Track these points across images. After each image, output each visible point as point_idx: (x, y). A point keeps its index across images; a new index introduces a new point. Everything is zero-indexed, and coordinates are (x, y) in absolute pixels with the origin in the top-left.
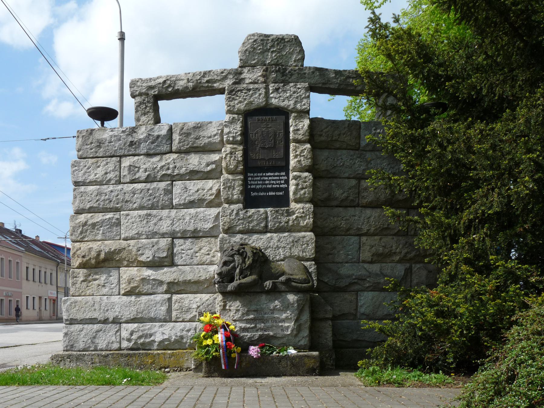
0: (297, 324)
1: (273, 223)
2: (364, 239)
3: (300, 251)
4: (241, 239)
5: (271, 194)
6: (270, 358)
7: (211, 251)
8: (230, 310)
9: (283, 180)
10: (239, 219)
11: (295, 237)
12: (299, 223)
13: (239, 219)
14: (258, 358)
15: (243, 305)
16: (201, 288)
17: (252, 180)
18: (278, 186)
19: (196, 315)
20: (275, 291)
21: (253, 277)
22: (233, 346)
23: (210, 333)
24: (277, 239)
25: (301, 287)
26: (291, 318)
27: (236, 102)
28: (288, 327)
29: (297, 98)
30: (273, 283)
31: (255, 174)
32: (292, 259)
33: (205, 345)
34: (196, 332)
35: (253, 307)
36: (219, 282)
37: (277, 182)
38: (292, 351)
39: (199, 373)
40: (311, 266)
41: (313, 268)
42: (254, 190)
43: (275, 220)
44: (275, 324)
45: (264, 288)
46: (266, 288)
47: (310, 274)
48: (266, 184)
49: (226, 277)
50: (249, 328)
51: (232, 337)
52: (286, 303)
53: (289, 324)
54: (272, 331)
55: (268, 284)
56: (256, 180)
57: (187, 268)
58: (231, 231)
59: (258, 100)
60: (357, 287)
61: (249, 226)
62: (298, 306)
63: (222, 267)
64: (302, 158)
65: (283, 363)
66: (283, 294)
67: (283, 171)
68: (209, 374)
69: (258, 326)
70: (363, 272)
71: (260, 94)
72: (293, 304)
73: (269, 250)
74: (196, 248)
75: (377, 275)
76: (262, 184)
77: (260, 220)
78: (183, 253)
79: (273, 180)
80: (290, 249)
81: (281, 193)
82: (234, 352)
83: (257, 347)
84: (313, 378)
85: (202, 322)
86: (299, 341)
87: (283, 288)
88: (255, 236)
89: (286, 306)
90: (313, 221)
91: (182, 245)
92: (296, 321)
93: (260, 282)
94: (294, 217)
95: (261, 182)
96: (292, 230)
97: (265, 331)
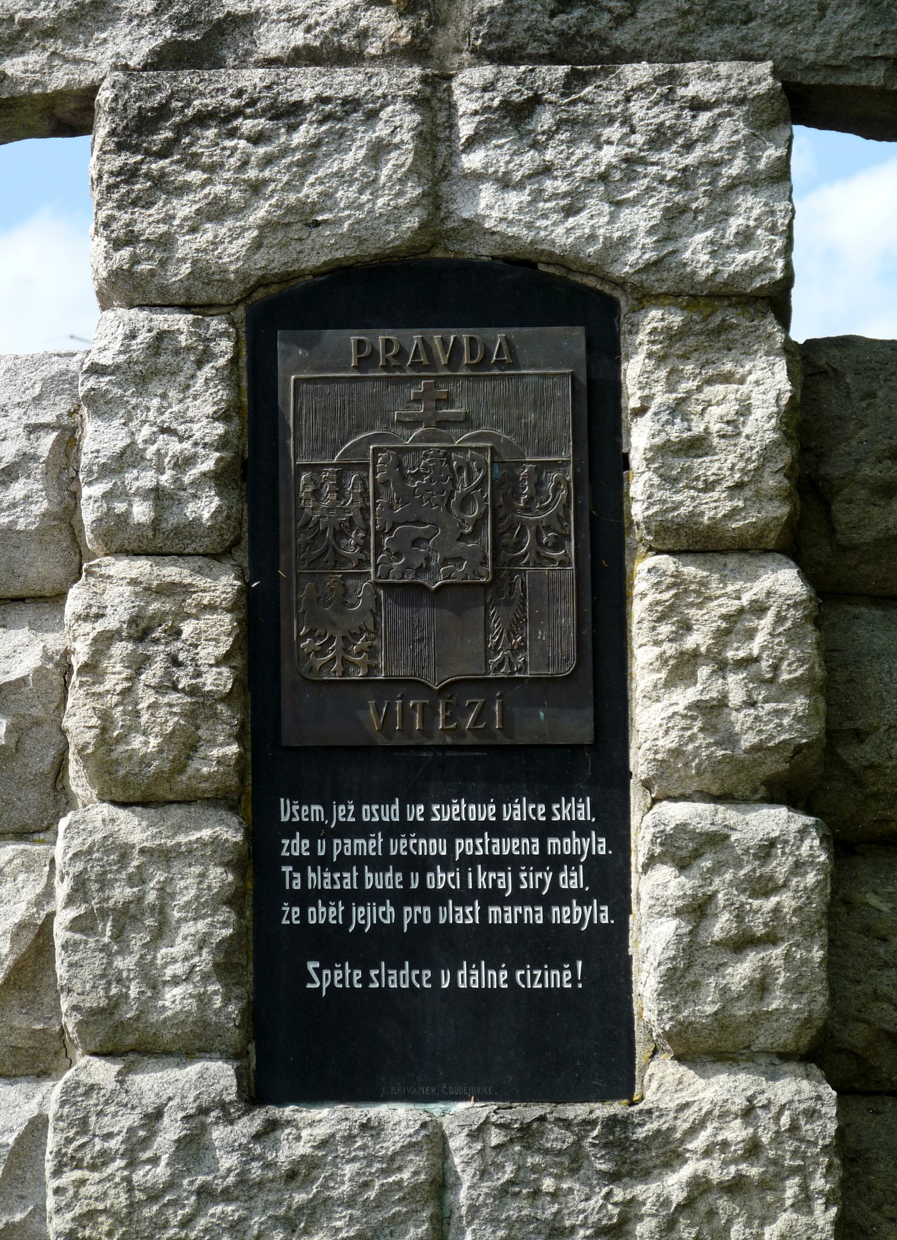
5: (474, 977)
9: (572, 861)
17: (314, 860)
18: (534, 915)
27: (184, 208)
29: (684, 180)
31: (343, 812)
37: (529, 880)
42: (334, 944)
48: (436, 899)
56: (344, 863)
59: (363, 195)
64: (735, 687)
67: (571, 793)
71: (378, 151)
76: (402, 898)
79: (493, 863)
81: (561, 978)
95: (391, 879)
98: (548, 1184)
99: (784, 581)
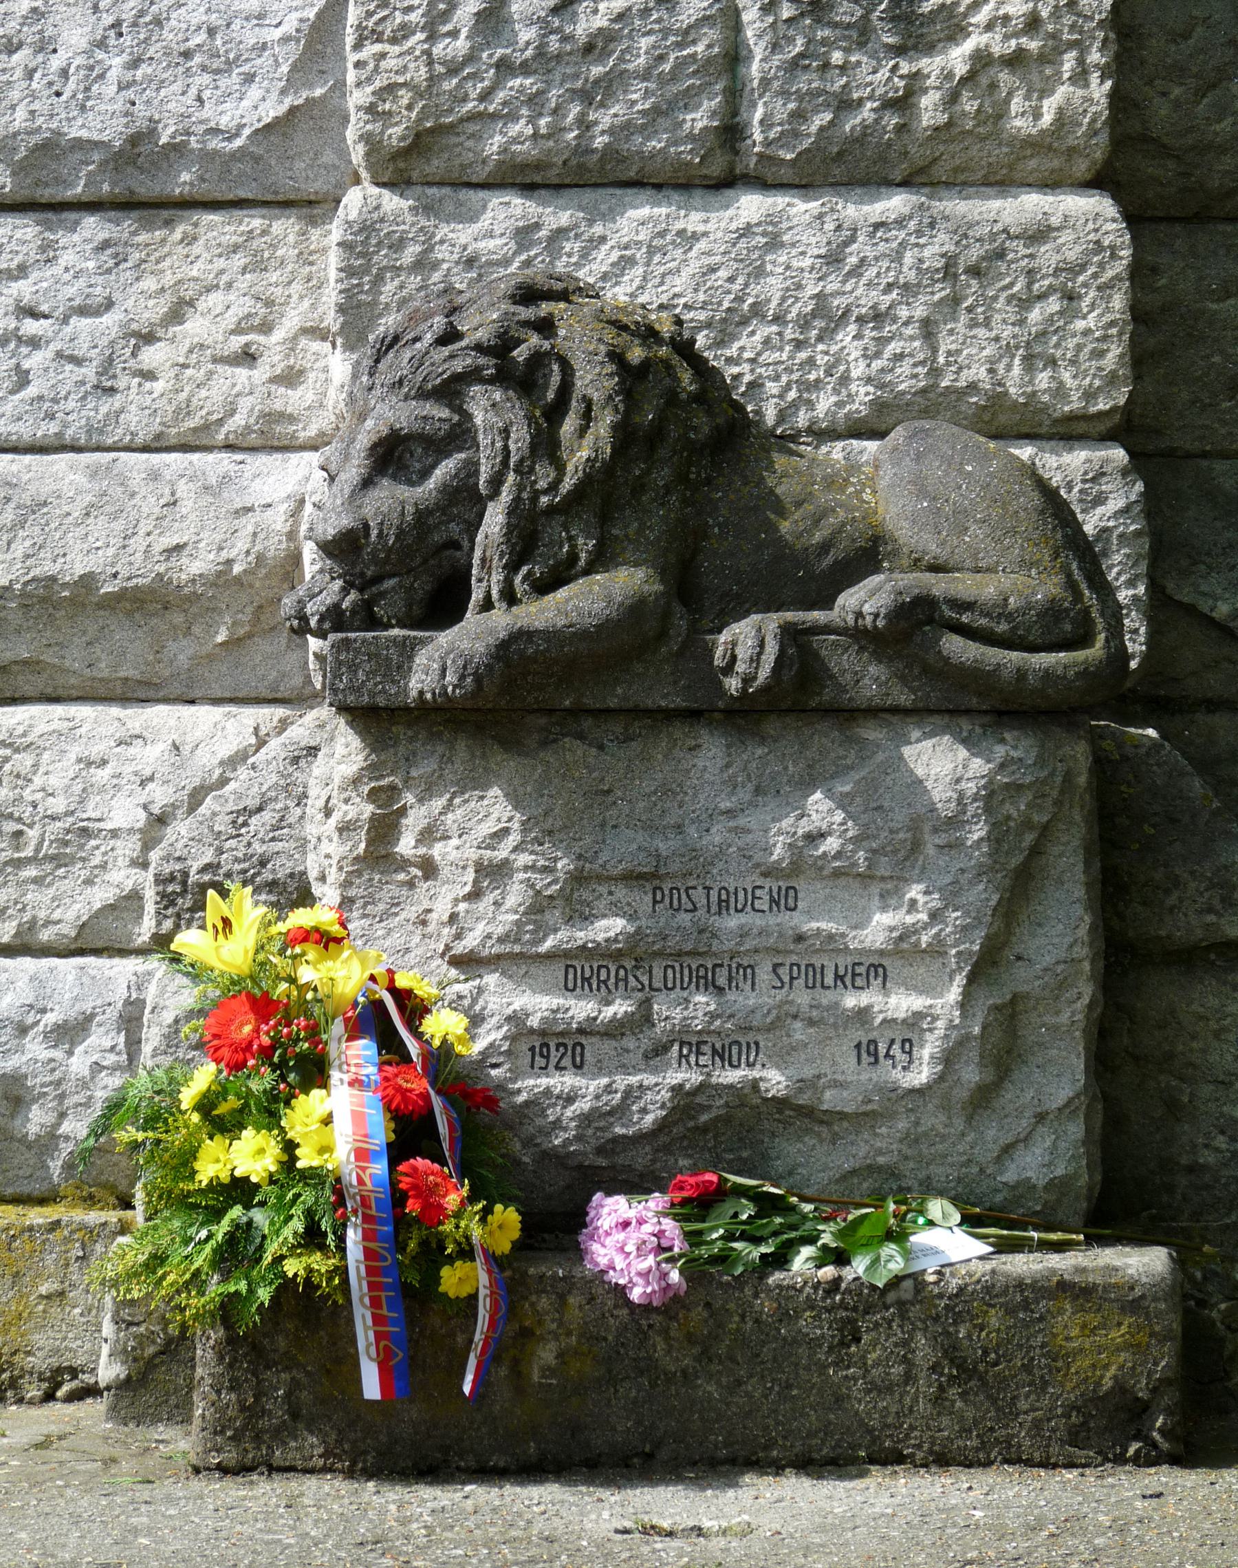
0: (986, 1000)
1: (783, 108)
3: (1009, 350)
4: (524, 235)
6: (766, 1306)
7: (266, 328)
8: (429, 869)
10: (504, 67)
11: (962, 232)
12: (1001, 113)
13: (504, 67)
14: (670, 1306)
15: (541, 829)
16: (182, 652)
19: (135, 897)
20: (801, 705)
21: (626, 582)
22: (452, 1200)
23: (261, 1082)
24: (815, 243)
25: (1021, 674)
26: (937, 950)
28: (915, 1021)
30: (790, 634)
32: (943, 429)
33: (215, 1187)
34: (134, 1044)
35: (624, 849)
36: (335, 619)
38: (948, 1245)
39: (161, 1431)
40: (1100, 487)
41: (1115, 503)
43: (805, 82)
44: (802, 998)
45: (713, 678)
46: (733, 684)
47: (1084, 553)
49: (399, 574)
50: (587, 1029)
51: (449, 1117)
52: (900, 817)
53: (917, 1002)
54: (781, 1059)
55: (747, 643)
57: (63, 470)
58: (436, 165)
61: (585, 125)
62: (996, 838)
63: (367, 483)
65: (876, 1348)
66: (872, 733)
68: (249, 1449)
69: (668, 1012)
72: (955, 822)
73: (749, 341)
74: (141, 302)
77: (674, 76)
78: (35, 343)
80: (928, 330)
82: (466, 1252)
83: (657, 1201)
84: (1126, 1488)
85: (196, 973)
86: (1007, 1150)
87: (871, 679)
88: (639, 217)
89: (899, 843)
90: (1114, 96)
91: (22, 271)
92: (984, 968)
93: (681, 623)
94: (957, 57)
96: (940, 172)
97: (723, 1056)
98: (837, 57)
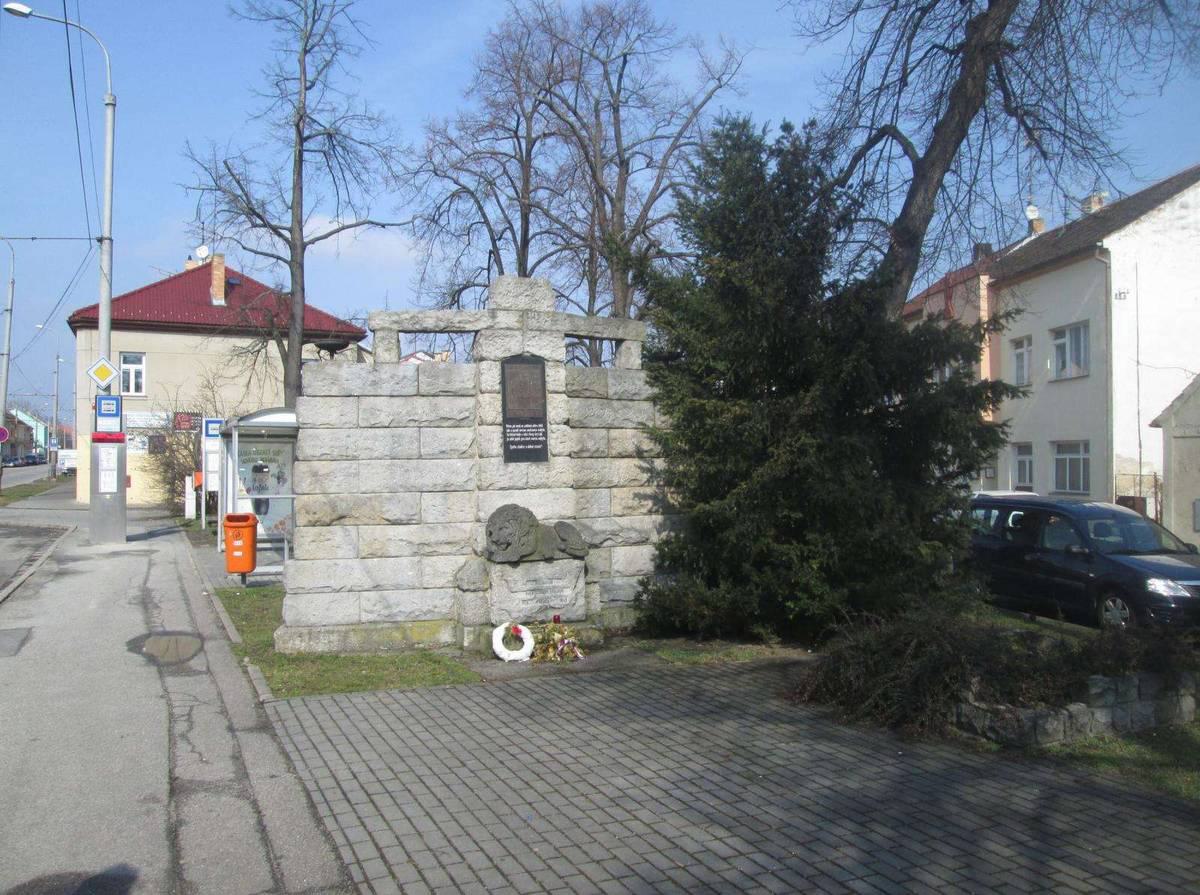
2: (615, 490)
5: (530, 447)
35: (532, 577)
42: (513, 443)
60: (609, 543)
70: (616, 527)
75: (629, 529)
81: (539, 447)
99: (564, 396)
